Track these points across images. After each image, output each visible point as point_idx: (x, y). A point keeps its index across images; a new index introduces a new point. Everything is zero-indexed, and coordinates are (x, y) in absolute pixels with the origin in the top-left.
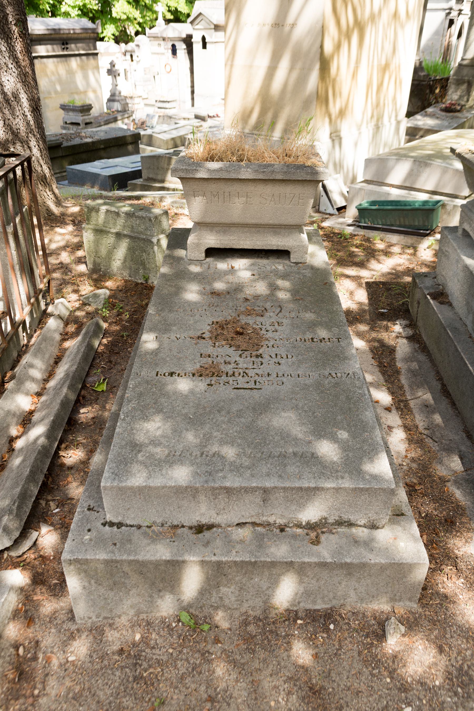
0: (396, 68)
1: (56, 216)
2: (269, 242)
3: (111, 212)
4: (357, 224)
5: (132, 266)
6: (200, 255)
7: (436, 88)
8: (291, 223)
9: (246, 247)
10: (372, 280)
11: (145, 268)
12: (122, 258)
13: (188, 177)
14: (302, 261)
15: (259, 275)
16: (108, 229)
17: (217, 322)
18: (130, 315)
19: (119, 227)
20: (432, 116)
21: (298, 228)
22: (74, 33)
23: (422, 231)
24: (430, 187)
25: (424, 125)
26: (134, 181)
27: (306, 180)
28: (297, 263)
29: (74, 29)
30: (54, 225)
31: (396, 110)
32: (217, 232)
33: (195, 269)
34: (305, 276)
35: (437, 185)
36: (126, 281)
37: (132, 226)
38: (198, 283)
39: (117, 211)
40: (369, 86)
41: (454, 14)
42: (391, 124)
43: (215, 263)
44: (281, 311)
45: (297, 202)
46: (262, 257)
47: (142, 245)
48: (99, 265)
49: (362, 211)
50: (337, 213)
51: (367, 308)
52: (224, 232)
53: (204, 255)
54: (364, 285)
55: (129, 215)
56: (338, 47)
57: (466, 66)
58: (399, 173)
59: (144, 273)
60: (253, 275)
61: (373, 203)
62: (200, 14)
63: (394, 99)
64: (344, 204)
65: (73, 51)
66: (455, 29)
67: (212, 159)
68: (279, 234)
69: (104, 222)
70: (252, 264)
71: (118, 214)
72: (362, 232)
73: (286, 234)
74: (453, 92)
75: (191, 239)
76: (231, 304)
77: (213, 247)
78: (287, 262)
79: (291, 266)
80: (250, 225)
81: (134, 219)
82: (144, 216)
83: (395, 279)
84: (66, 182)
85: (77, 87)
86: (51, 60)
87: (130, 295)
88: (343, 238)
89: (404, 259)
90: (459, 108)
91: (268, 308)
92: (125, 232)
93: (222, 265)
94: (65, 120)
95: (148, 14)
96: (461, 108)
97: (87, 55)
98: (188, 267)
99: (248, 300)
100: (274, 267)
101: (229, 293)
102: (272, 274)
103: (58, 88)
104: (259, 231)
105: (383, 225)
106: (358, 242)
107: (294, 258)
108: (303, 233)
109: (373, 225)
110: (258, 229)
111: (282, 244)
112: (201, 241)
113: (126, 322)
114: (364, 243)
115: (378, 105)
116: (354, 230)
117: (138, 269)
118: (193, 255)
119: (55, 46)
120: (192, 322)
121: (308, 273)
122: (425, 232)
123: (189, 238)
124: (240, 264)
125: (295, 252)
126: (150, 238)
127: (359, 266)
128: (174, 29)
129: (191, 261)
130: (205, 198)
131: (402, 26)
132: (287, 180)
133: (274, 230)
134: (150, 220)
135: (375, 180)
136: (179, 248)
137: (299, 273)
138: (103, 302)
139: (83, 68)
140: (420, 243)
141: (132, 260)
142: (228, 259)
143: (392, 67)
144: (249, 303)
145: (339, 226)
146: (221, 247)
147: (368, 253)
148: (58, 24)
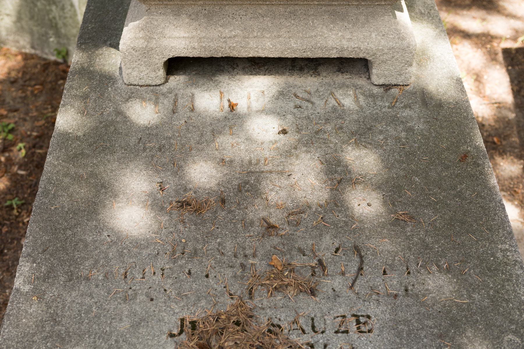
5: (35, 29)
6: (153, 75)
11: (58, 34)
15: (299, 130)
17: (193, 324)
18: (28, 149)
28: (387, 87)
32: (194, 17)
33: (143, 114)
36: (26, 57)
43: (189, 91)
44: (361, 269)
51: (512, 116)
53: (162, 73)
54: (500, 57)
59: (59, 43)
60: (284, 132)
68: (343, 18)
70: (281, 94)
76: (229, 246)
77: (182, 55)
78: (361, 82)
79: (372, 96)
87: (32, 92)
91: (327, 256)
93: (208, 100)
98: (123, 107)
99: (274, 227)
100: (332, 102)
101: (223, 201)
102: (329, 127)
104: (293, 13)
107: (379, 75)
108: (401, 10)
111: (352, 44)
112: (153, 44)
113: (20, 168)
117: (46, 35)
118: (135, 74)
120: (125, 325)
123: (125, 29)
124: (252, 91)
136: (105, 43)
137: (394, 120)
144: (276, 240)
146: (203, 55)
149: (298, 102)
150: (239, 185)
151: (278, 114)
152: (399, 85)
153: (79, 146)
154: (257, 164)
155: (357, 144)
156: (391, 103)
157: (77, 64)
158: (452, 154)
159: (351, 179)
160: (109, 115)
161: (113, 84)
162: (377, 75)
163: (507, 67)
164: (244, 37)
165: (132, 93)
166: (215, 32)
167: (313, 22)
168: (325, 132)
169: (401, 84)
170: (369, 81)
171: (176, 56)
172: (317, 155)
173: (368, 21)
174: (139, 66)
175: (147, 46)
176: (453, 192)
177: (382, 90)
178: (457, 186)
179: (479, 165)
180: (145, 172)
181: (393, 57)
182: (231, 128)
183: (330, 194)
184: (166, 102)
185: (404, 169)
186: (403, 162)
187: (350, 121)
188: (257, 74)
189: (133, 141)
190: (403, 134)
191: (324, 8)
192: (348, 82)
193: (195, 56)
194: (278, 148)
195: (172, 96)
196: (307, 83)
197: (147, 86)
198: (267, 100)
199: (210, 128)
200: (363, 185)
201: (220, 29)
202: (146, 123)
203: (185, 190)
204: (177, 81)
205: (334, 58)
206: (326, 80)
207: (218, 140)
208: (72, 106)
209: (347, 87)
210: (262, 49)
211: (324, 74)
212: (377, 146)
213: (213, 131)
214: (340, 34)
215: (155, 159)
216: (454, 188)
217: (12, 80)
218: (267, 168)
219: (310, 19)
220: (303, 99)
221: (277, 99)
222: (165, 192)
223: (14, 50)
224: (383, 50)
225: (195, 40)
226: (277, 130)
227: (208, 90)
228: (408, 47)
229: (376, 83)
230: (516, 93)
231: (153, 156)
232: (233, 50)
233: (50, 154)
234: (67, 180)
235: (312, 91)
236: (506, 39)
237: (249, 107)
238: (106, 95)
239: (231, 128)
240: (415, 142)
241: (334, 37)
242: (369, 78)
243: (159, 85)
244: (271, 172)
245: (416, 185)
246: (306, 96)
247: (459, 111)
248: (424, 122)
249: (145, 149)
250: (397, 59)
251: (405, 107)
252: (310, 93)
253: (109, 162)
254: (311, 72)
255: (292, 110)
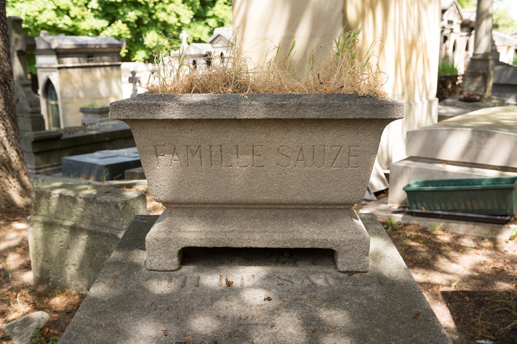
0: (422, 46)
1: (19, 208)
2: (297, 236)
3: (65, 197)
4: (405, 208)
5: (91, 274)
7: (448, 84)
8: (336, 200)
9: (253, 245)
10: (452, 289)
12: (77, 263)
13: (142, 117)
14: (360, 268)
15: (280, 298)
16: (60, 221)
19: (75, 218)
20: (452, 105)
21: (345, 208)
22: (100, 48)
23: (499, 217)
24: (499, 161)
25: (446, 113)
26: (132, 170)
27: (361, 120)
28: (350, 273)
29: (99, 45)
30: (12, 219)
31: (426, 89)
32: (204, 218)
33: (161, 287)
34: (371, 298)
35: (510, 159)
37: (93, 216)
38: (156, 319)
39: (72, 195)
40: (398, 60)
41: (446, 32)
42: (423, 103)
45: (345, 162)
46: (284, 263)
47: (105, 243)
48: (47, 272)
49: (410, 193)
50: (375, 198)
52: (215, 219)
53: (176, 260)
54: (440, 296)
55: (89, 200)
56: (362, 16)
57: (479, 60)
58: (454, 146)
60: (269, 299)
61: (426, 183)
62: (219, 35)
63: (424, 77)
64: (383, 188)
65: (99, 62)
66: (450, 44)
67: (189, 90)
69: (56, 212)
70: (269, 277)
71: (73, 200)
72: (415, 221)
73: (328, 220)
74: (469, 84)
75: (155, 232)
77: (193, 245)
78: (331, 270)
79: (338, 278)
80: (260, 204)
81: (95, 205)
82: (109, 200)
83: (483, 285)
84: (61, 174)
85: (99, 93)
86: (76, 70)
88: (390, 228)
89: (483, 254)
90: (478, 98)
92: (83, 226)
93: (212, 280)
94: (84, 122)
95: (175, 42)
96: (480, 98)
97: (111, 66)
98: (144, 284)
102: (305, 297)
103: (81, 94)
105: (442, 210)
106: (412, 233)
107: (343, 262)
109: (428, 212)
110: (274, 212)
112: (172, 236)
114: (420, 234)
115: (408, 83)
116: (403, 219)
118: (156, 260)
119: (81, 59)
121: (374, 292)
122: (503, 218)
124: (246, 275)
125: (346, 252)
126: (115, 233)
127: (424, 267)
128: (195, 48)
129: (157, 273)
130: (175, 157)
131: (425, 7)
132: (326, 120)
133: (305, 212)
134: (117, 207)
135: (423, 156)
136: (137, 247)
137: (357, 293)
138: (31, 335)
139: (107, 77)
140: (498, 233)
141: (91, 266)
142: (221, 267)
143: (419, 44)
145: (383, 214)
146: (208, 245)
147: (430, 248)
148: (86, 41)
149: (281, 281)
150: (230, 333)
151: (265, 288)
152: (360, 272)
153: (104, 306)
154: (245, 319)
155: (328, 307)
156: (354, 283)
157: (113, 258)
158: (406, 314)
159: (323, 330)
160: (131, 288)
161: (138, 270)
162: (341, 262)
163: (447, 303)
164: (240, 232)
165: (152, 275)
166: (217, 228)
167: (291, 222)
168: (302, 300)
169: (361, 270)
170: (336, 270)
171: (188, 246)
172: (295, 314)
173: (332, 222)
174: (159, 254)
175: (166, 237)
176: (409, 339)
177: (346, 275)
178: (413, 335)
179: (429, 321)
180: (153, 324)
181: (353, 247)
182: (226, 297)
183: (306, 339)
184: (177, 281)
185: (367, 324)
186: (366, 319)
187: (322, 293)
188: (251, 265)
189: (147, 304)
190: (365, 302)
191: (299, 212)
192: (319, 270)
193: (202, 246)
194: (264, 309)
195: (183, 278)
196: (287, 271)
197: (164, 271)
198: (256, 280)
199: (210, 297)
200: (333, 334)
201: (222, 226)
202: (160, 293)
203: (185, 335)
204: (188, 269)
205: (308, 248)
206: (302, 269)
207: (215, 304)
208: (104, 283)
209: (319, 273)
210: (253, 240)
211: (301, 266)
212: (345, 308)
213: (212, 299)
214: (311, 230)
215: (163, 315)
216: (411, 336)
217: (68, 311)
218: (254, 322)
219: (289, 220)
220: (284, 280)
221: (264, 279)
222: (167, 337)
223: (74, 292)
224: (344, 241)
225: (203, 233)
226: (263, 298)
227: (211, 274)
228: (364, 239)
229: (341, 270)
230: (456, 321)
231: (161, 314)
232: (231, 241)
233: (79, 311)
234: (88, 328)
235: (292, 275)
236: (443, 286)
237: (241, 285)
238: (132, 276)
239: (226, 297)
240: (375, 306)
241: (307, 232)
242: (336, 268)
243: (174, 271)
244: (257, 324)
245: (378, 334)
246: (287, 278)
247: (408, 287)
248: (381, 294)
249: (156, 309)
250: (355, 250)
251: (365, 285)
252: (290, 277)
253: (125, 317)
254: (291, 264)
255: (276, 286)
